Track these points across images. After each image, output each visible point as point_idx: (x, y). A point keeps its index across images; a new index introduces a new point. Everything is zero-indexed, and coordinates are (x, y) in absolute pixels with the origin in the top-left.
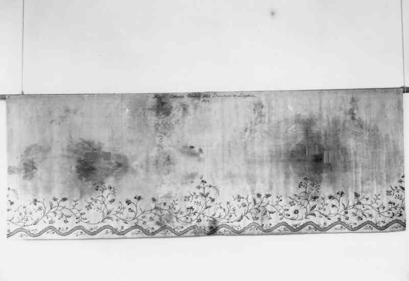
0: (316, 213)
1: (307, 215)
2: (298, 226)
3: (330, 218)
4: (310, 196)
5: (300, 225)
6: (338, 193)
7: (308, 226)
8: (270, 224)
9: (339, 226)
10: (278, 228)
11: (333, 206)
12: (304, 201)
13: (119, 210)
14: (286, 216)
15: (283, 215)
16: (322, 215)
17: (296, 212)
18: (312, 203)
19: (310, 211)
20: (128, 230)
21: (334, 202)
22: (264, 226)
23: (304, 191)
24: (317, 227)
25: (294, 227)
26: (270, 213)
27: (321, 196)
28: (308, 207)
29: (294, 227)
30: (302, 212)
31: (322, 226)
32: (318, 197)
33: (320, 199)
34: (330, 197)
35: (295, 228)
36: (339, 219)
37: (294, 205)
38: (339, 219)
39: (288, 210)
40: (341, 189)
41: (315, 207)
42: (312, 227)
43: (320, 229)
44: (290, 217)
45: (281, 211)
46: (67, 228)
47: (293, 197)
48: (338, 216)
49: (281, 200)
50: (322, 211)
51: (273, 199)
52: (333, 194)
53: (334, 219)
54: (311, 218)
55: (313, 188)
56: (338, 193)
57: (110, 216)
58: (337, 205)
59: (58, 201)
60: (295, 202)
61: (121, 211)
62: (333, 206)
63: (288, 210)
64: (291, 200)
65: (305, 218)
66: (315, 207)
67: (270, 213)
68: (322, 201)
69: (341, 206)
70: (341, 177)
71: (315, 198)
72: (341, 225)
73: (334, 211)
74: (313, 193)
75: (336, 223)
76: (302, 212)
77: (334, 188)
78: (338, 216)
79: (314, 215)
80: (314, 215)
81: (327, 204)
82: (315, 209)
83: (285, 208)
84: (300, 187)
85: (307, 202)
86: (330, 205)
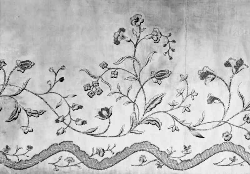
0: (160, 117)
1: (134, 124)
2: (108, 155)
3: (202, 133)
4: (146, 70)
5: (115, 151)
6: (227, 64)
7: (139, 154)
8: (30, 148)
9: (226, 156)
10: (51, 160)
11: (212, 99)
12: (128, 83)
13: (179, 100)
14: (73, 124)
15: (67, 120)
16: (177, 124)
17: (105, 113)
18: (152, 90)
19: (145, 112)
20: (203, 157)
21: (215, 88)
22: (10, 152)
23: (131, 54)
24: (165, 160)
25: (96, 157)
26: (30, 114)
27: (178, 71)
28: (140, 102)
29: (96, 157)
30: (122, 115)
31: (178, 154)
32: (169, 73)
33: (175, 77)
34: (204, 75)
35: (100, 159)
36: (228, 137)
37: (100, 92)
38: (228, 137)
39: (80, 107)
40: (234, 55)
41: (157, 101)
42: (149, 157)
43: (171, 165)
44: (85, 128)
45: (64, 110)
46: (30, 148)
47: (99, 71)
48: (226, 128)
49: (62, 80)
50: (178, 113)
51: (38, 77)
52: (212, 67)
53: (214, 137)
54: (148, 133)
55: (156, 47)
56: (227, 64)
57: (154, 117)
58: (224, 98)
59: (8, 68)
60: (102, 85)
61: (185, 104)
62: (212, 99)
63: (80, 107)
64: (90, 81)
65: (131, 131)
66: (157, 101)
67: (30, 114)
68: (182, 85)
69: (235, 96)
70: (237, 17)
71: (160, 76)
72: (232, 155)
73: (214, 112)
74: (155, 63)
75: (217, 149)
76: (122, 115)
77: (217, 49)
78: (226, 128)
79: (157, 123)
80: (157, 123)
81: (194, 95)
82: (159, 107)
83: (71, 101)
84: (117, 42)
85: (136, 86)
86: (203, 99)
